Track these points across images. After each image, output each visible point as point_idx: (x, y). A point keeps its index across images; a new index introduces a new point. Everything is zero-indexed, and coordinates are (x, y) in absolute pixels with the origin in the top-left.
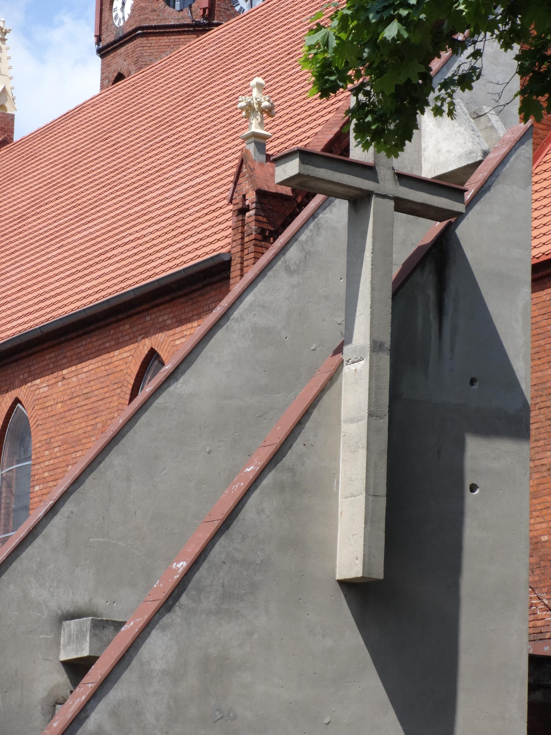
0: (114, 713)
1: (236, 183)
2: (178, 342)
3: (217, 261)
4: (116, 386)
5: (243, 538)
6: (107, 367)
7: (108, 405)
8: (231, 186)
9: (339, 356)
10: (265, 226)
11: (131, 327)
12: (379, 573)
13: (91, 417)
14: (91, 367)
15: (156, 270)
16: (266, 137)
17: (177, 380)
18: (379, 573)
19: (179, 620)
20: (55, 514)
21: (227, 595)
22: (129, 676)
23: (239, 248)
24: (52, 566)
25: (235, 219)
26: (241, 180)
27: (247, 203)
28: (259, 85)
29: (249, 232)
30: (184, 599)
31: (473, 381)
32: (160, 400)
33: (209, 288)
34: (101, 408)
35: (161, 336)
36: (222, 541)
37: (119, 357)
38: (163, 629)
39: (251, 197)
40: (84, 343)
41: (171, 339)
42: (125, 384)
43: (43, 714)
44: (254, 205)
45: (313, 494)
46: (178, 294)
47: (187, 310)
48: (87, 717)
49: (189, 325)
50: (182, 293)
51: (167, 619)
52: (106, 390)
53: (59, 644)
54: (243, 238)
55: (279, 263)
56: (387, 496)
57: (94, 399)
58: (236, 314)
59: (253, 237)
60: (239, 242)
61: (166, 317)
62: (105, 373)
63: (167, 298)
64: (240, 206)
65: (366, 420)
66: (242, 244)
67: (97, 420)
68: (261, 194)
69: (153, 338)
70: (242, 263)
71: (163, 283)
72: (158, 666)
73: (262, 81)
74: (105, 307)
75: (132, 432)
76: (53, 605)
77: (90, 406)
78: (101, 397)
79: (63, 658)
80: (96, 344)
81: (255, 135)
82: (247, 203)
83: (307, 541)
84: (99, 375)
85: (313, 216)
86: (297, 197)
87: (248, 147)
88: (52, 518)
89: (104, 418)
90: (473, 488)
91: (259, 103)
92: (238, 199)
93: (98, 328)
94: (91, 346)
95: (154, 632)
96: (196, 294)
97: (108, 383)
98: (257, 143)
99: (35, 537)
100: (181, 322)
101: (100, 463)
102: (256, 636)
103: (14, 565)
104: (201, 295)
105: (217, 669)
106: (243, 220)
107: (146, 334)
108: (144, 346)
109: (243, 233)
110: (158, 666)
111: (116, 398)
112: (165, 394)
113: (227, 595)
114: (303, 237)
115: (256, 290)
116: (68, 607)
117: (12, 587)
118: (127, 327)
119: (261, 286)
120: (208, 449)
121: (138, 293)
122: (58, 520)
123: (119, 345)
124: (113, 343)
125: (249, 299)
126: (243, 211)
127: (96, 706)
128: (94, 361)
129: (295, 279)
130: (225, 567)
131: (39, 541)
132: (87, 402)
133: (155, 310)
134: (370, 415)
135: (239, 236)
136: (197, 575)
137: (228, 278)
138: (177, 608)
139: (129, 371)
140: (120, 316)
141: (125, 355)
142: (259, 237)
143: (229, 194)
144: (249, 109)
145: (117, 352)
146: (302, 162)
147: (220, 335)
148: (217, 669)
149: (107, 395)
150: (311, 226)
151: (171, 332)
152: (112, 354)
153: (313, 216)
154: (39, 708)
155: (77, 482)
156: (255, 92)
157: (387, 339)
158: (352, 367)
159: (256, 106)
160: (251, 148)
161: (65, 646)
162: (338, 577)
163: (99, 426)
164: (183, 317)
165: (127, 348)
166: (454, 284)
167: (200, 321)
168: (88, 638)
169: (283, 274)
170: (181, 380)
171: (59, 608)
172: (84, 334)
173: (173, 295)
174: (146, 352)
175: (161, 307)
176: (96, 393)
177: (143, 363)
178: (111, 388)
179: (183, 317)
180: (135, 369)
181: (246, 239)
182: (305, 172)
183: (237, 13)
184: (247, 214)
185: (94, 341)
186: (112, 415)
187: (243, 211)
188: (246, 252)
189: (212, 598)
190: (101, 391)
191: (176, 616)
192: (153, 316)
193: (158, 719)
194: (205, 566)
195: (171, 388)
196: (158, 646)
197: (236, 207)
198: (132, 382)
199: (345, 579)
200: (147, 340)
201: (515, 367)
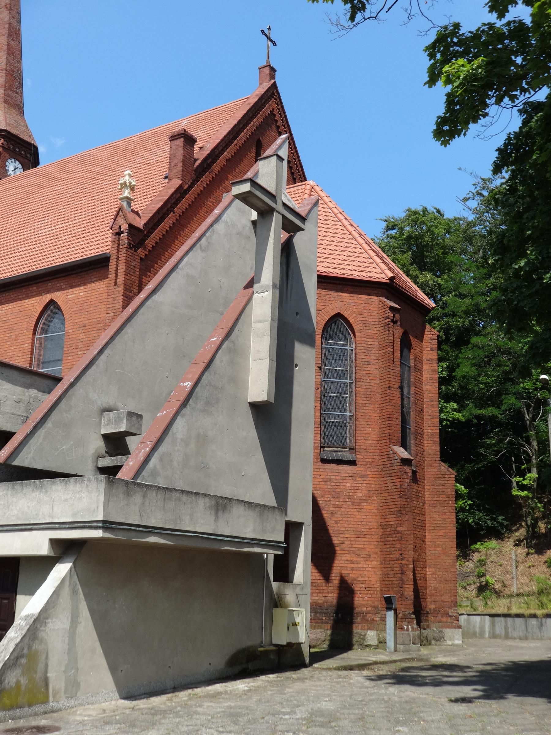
0: (161, 459)
1: (115, 220)
2: (69, 297)
3: (102, 256)
4: (25, 317)
5: (215, 374)
6: (20, 308)
7: (20, 327)
8: (112, 221)
9: (249, 290)
10: (131, 242)
11: (38, 288)
12: (273, 400)
13: (7, 332)
14: (8, 308)
15: (56, 261)
16: (131, 200)
17: (156, 294)
18: (273, 400)
19: (188, 412)
20: (102, 354)
21: (208, 403)
22: (168, 439)
23: (116, 251)
24: (100, 381)
25: (114, 237)
26: (118, 219)
27: (122, 230)
28: (129, 175)
29: (123, 244)
30: (191, 401)
31: (297, 314)
32: (149, 303)
33: (92, 271)
34: (15, 328)
35: (58, 294)
36: (206, 374)
37: (29, 303)
38: (183, 416)
39: (125, 227)
40: (4, 295)
41: (65, 295)
42: (33, 316)
43: (93, 463)
44: (127, 231)
45: (239, 355)
46: (73, 272)
47: (76, 281)
48: (150, 460)
49: (78, 288)
50: (75, 272)
51: (184, 411)
52: (19, 319)
53: (101, 424)
54: (118, 247)
55: (198, 245)
56: (276, 361)
57: (10, 323)
58: (180, 266)
59: (125, 246)
60: (116, 248)
61: (62, 284)
62: (18, 311)
63: (64, 274)
64: (118, 231)
65: (269, 321)
66: (118, 250)
67: (11, 334)
68: (131, 227)
69: (52, 294)
70: (117, 259)
71: (93, 259)
72: (179, 436)
73: (131, 173)
74: (25, 277)
75: (136, 317)
76: (99, 403)
77: (6, 327)
78: (15, 323)
79: (103, 432)
80: (12, 296)
81: (127, 198)
82: (122, 230)
83: (238, 380)
84: (14, 311)
85: (211, 225)
86: (145, 230)
87: (122, 203)
88: (100, 356)
89: (17, 333)
90: (297, 366)
91: (130, 183)
92: (116, 227)
93: (14, 288)
94: (9, 297)
95: (179, 417)
96: (83, 273)
97: (20, 316)
98: (128, 202)
99: (93, 365)
100: (72, 287)
101: (122, 330)
102: (218, 426)
103: (83, 378)
104: (87, 274)
105: (203, 441)
106: (119, 238)
107: (48, 292)
108: (47, 298)
109: (119, 245)
110: (179, 436)
111: (25, 323)
112: (150, 300)
113: (208, 403)
114: (207, 235)
115: (189, 255)
116: (106, 405)
117: (81, 390)
118: (35, 288)
119: (191, 254)
120: (167, 332)
121: (47, 271)
122: (103, 357)
123: (28, 297)
124: (24, 296)
125: (186, 260)
126: (119, 233)
127: (113, 668)
128: (11, 304)
129: (204, 254)
130: (207, 387)
131: (94, 367)
132: (5, 324)
133: (54, 280)
134: (272, 320)
135: (116, 245)
136: (197, 390)
137: (108, 265)
138: (188, 406)
139: (35, 310)
140: (31, 283)
141: (32, 302)
142: (129, 247)
143: (110, 225)
144: (124, 185)
145: (27, 301)
146: (251, 185)
147: (174, 274)
148: (203, 441)
149: (19, 322)
150: (211, 230)
151: (66, 291)
152: (23, 301)
153: (211, 225)
154: (91, 459)
155: (112, 338)
156: (127, 177)
157: (278, 283)
158: (260, 295)
159: (128, 184)
160: (125, 204)
161: (104, 426)
162: (249, 401)
163: (13, 337)
164: (74, 284)
165: (34, 299)
166: (292, 265)
167: (85, 287)
168: (125, 421)
169: (199, 250)
170: (157, 294)
171: (102, 405)
172: (4, 291)
173: (68, 273)
174: (48, 301)
175: (59, 279)
176: (12, 320)
177: (45, 306)
178: (23, 318)
179: (74, 284)
180: (40, 310)
181: (121, 247)
182: (252, 190)
183: (9, 176)
184: (122, 235)
185: (12, 294)
186: (22, 332)
187: (119, 233)
188: (120, 253)
189: (202, 403)
190: (15, 319)
191: (187, 411)
192: (53, 283)
193: (179, 465)
194: (199, 385)
195: (153, 298)
196: (180, 425)
197: (115, 231)
198: (37, 315)
199: (254, 402)
200: (48, 295)
201: (311, 311)
